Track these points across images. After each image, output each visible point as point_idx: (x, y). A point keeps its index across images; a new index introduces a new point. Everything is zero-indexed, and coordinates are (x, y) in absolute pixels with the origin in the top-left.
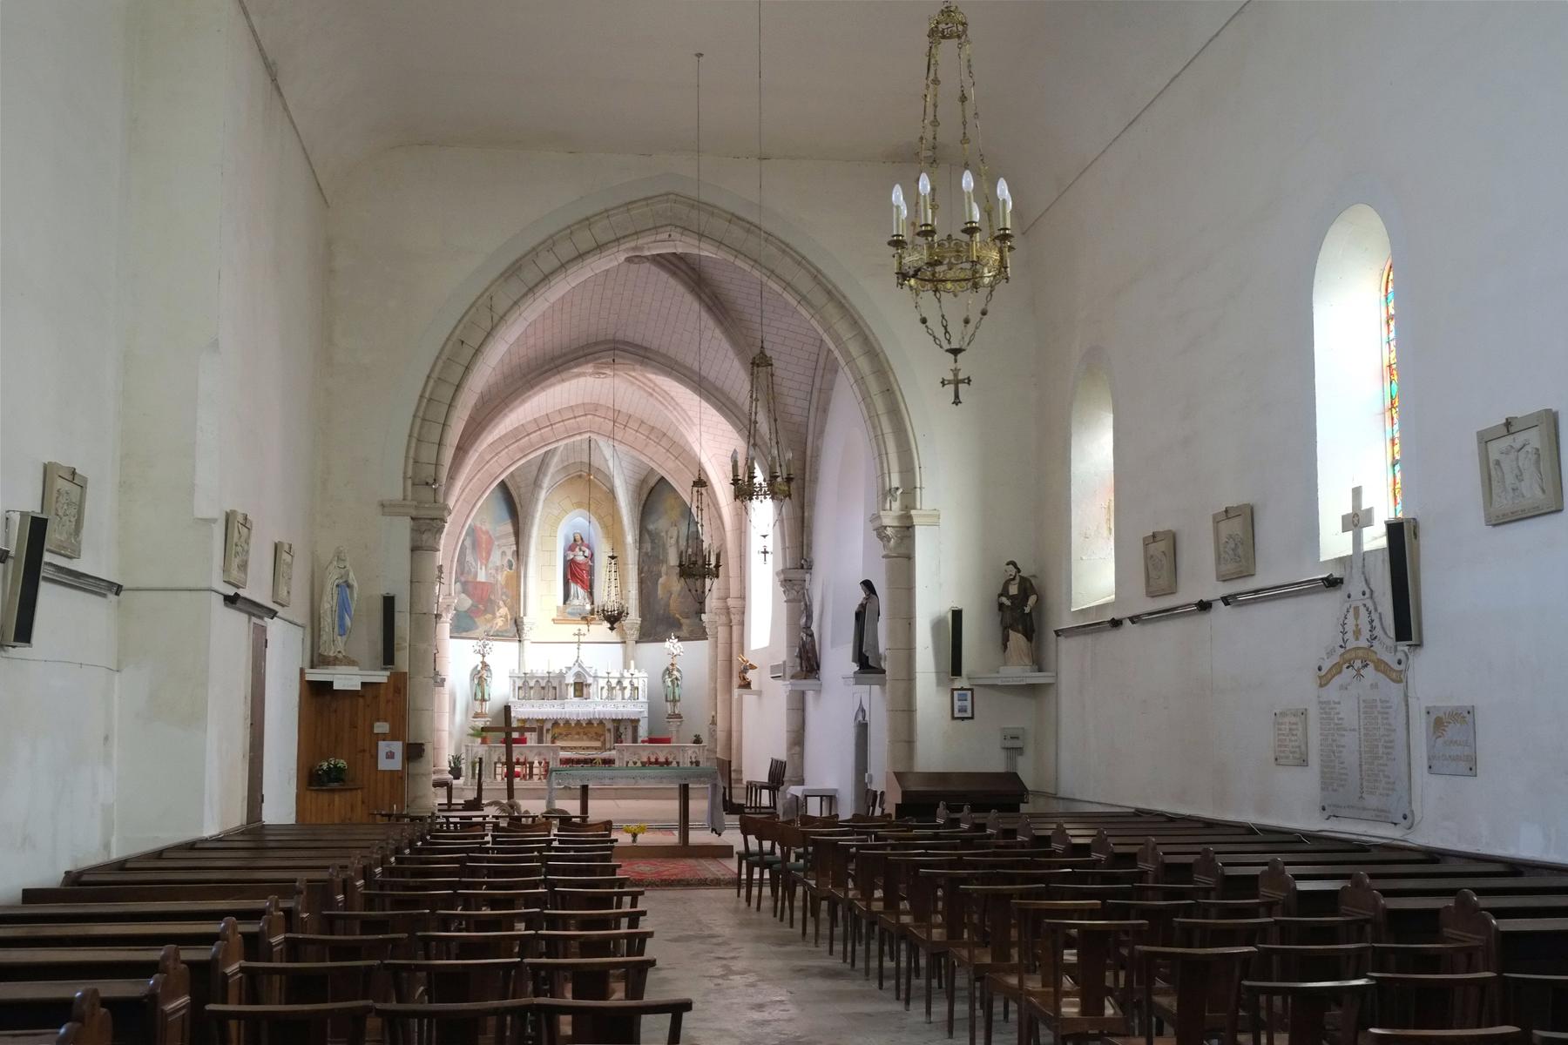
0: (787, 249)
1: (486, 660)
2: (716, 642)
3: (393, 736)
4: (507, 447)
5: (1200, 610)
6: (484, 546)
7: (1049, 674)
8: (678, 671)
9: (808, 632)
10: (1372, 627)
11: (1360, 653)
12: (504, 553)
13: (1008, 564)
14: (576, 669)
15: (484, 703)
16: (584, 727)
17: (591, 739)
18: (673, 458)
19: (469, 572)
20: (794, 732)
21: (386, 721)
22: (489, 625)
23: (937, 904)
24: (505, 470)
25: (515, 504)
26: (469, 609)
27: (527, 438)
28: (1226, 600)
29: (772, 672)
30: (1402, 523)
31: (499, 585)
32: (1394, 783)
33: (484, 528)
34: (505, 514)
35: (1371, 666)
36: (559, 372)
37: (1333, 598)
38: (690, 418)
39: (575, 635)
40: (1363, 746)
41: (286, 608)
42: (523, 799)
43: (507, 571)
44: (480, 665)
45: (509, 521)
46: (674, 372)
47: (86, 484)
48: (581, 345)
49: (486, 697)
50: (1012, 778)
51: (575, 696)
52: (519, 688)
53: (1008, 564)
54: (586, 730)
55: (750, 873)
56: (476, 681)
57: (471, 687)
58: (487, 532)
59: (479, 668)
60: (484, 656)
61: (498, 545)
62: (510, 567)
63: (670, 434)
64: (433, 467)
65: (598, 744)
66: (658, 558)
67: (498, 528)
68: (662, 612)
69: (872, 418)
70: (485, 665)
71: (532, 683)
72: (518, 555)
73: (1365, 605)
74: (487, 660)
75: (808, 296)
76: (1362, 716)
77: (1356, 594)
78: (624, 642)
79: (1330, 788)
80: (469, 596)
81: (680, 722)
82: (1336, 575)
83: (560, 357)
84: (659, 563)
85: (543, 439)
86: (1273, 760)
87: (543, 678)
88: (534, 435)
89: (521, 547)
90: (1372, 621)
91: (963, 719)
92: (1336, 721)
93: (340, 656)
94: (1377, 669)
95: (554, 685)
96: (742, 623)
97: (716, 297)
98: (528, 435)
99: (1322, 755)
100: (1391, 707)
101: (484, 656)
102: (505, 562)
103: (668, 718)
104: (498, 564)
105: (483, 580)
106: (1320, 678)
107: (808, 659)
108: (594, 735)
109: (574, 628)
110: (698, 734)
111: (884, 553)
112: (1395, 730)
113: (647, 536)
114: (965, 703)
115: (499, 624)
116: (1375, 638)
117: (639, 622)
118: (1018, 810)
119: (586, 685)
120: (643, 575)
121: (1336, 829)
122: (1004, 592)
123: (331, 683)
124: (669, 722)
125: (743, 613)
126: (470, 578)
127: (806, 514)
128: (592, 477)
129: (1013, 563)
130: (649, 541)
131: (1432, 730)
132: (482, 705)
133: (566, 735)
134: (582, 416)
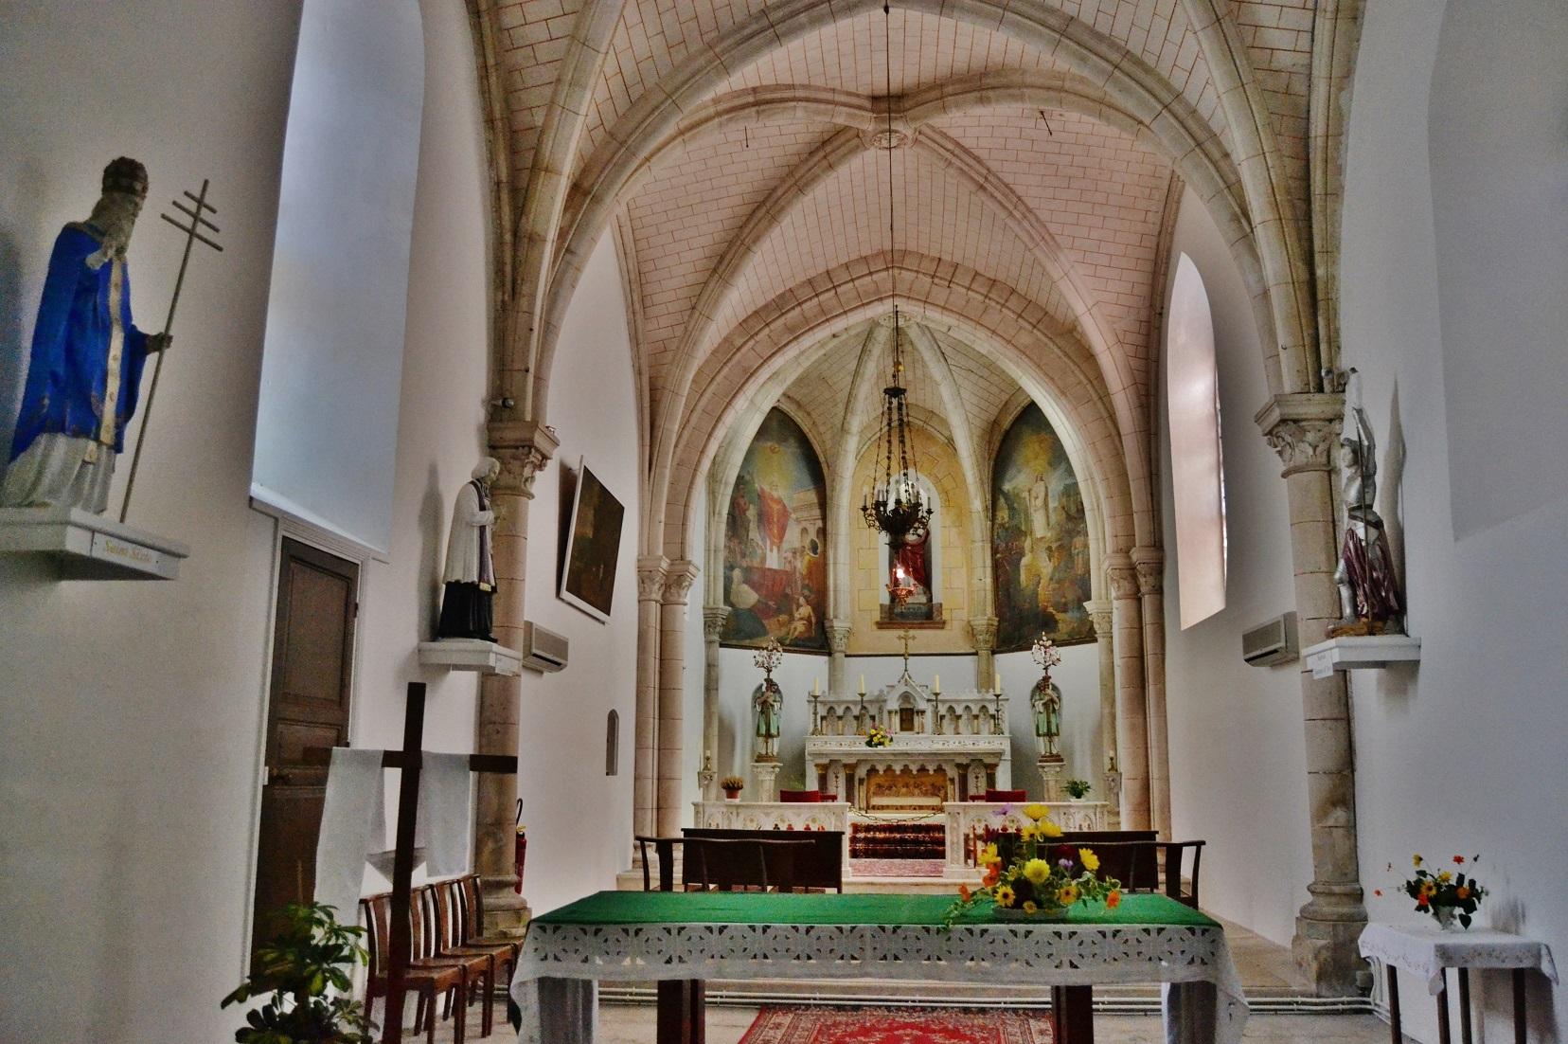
1: (772, 676)
2: (1111, 643)
6: (775, 520)
9: (1370, 517)
12: (804, 530)
14: (903, 689)
15: (770, 740)
16: (914, 777)
17: (925, 794)
18: (1030, 327)
22: (784, 630)
23: (532, 419)
26: (753, 606)
27: (798, 310)
31: (798, 575)
33: (775, 494)
34: (805, 478)
36: (778, 38)
43: (809, 555)
44: (765, 685)
46: (1009, 15)
49: (773, 731)
51: (902, 729)
52: (823, 718)
56: (759, 709)
57: (754, 715)
58: (779, 501)
60: (769, 671)
62: (814, 549)
71: (840, 711)
74: (774, 676)
78: (976, 654)
81: (1061, 767)
87: (855, 703)
88: (808, 303)
89: (829, 524)
95: (872, 713)
98: (800, 304)
101: (769, 671)
102: (807, 543)
103: (1040, 761)
104: (797, 544)
108: (929, 787)
110: (1462, 864)
113: (1002, 500)
117: (996, 623)
119: (918, 712)
120: (999, 555)
124: (1043, 767)
126: (756, 563)
127: (1320, 272)
132: (767, 743)
133: (890, 788)
134: (883, 270)
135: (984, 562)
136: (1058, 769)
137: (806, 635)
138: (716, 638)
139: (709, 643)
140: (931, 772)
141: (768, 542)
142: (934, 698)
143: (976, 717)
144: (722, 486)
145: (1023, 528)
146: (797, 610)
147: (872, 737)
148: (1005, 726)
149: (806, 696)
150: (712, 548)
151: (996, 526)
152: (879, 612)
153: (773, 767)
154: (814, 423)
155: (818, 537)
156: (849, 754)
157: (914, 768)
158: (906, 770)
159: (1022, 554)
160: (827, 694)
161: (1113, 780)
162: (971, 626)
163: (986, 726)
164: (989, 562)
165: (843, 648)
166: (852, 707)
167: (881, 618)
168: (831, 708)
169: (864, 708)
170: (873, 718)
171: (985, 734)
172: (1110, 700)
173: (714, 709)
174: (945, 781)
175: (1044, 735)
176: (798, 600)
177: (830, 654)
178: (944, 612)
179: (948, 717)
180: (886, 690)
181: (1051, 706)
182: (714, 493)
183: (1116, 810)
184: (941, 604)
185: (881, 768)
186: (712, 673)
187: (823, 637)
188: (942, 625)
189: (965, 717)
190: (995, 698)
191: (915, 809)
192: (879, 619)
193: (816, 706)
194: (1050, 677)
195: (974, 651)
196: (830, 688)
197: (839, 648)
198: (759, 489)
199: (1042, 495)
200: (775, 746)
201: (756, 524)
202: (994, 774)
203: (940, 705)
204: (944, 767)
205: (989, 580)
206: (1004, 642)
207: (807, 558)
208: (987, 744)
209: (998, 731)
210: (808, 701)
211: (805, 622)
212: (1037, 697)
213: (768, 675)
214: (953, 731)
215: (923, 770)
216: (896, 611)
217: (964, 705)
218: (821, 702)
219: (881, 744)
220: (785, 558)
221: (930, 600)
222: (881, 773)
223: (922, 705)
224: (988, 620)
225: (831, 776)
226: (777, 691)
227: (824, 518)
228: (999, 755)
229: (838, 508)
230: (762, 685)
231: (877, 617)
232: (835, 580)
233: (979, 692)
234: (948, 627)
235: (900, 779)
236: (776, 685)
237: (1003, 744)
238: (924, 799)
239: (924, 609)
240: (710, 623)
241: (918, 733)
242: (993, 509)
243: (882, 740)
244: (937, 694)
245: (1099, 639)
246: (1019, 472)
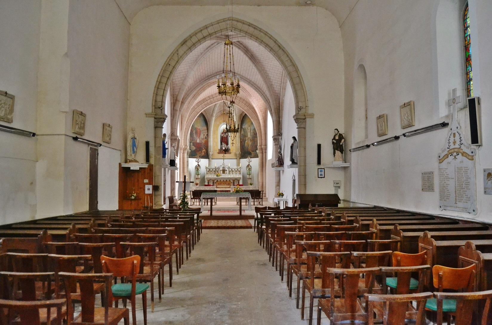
0: (266, 33)
1: (199, 164)
3: (149, 184)
4: (201, 104)
5: (396, 139)
7: (348, 163)
8: (251, 166)
10: (461, 140)
11: (456, 150)
12: (204, 135)
13: (335, 130)
14: (223, 166)
17: (227, 185)
19: (195, 140)
20: (277, 182)
21: (147, 179)
24: (201, 111)
25: (207, 121)
28: (404, 135)
29: (272, 165)
30: (474, 99)
32: (469, 198)
33: (199, 128)
34: (204, 124)
35: (460, 154)
37: (445, 130)
38: (250, 94)
39: (223, 157)
40: (456, 184)
41: (110, 144)
43: (205, 140)
45: (206, 126)
47: (86, 116)
48: (216, 72)
49: (199, 174)
50: (336, 196)
53: (335, 130)
55: (258, 224)
56: (196, 170)
57: (195, 171)
58: (199, 129)
59: (197, 166)
60: (198, 163)
61: (203, 133)
63: (245, 100)
64: (161, 103)
67: (202, 128)
70: (198, 165)
71: (211, 170)
72: (208, 135)
73: (458, 132)
75: (273, 48)
76: (456, 173)
77: (454, 128)
78: (237, 159)
79: (443, 200)
80: (194, 146)
82: (446, 122)
83: (210, 76)
85: (211, 102)
86: (421, 189)
87: (214, 168)
90: (461, 138)
91: (321, 178)
92: (446, 175)
93: (133, 159)
94: (462, 155)
96: (266, 152)
97: (252, 56)
98: (207, 101)
99: (440, 188)
100: (468, 169)
101: (198, 163)
102: (205, 137)
105: (199, 142)
106: (440, 160)
107: (280, 161)
109: (222, 155)
111: (297, 127)
112: (470, 178)
113: (242, 130)
114: (322, 173)
116: (462, 144)
118: (337, 206)
121: (445, 214)
122: (334, 139)
123: (130, 168)
125: (266, 150)
127: (280, 120)
128: (224, 112)
129: (337, 130)
131: (486, 177)
133: (220, 184)
148: (242, 173)
156: (213, 178)
157: (225, 180)
159: (246, 140)
163: (238, 173)
166: (214, 169)
170: (217, 171)
177: (209, 159)
204: (230, 180)
209: (240, 174)
215: (227, 181)
223: (227, 169)
227: (208, 132)
231: (218, 151)
234: (232, 153)
237: (241, 176)
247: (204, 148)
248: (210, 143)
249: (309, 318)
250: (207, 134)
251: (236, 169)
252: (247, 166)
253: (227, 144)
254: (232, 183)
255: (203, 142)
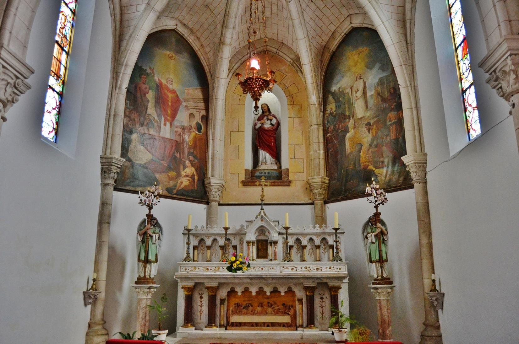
1: (152, 212)
6: (170, 104)
12: (192, 115)
14: (259, 223)
15: (148, 265)
16: (268, 298)
17: (277, 313)
31: (185, 145)
33: (171, 87)
42: (450, 155)
43: (195, 133)
49: (151, 257)
51: (258, 257)
52: (195, 248)
54: (272, 300)
58: (174, 92)
60: (150, 208)
61: (186, 106)
62: (199, 128)
65: (286, 319)
66: (344, 115)
68: (351, 166)
69: (485, 64)
70: (151, 218)
71: (209, 242)
78: (312, 204)
84: (345, 119)
87: (220, 235)
102: (194, 124)
103: (373, 284)
104: (186, 124)
108: (281, 306)
113: (331, 98)
115: (184, 184)
117: (327, 182)
119: (271, 243)
124: (376, 289)
130: (333, 101)
132: (145, 267)
133: (246, 307)
135: (319, 140)
136: (389, 290)
137: (190, 188)
138: (112, 182)
139: (104, 186)
140: (283, 294)
141: (163, 119)
142: (284, 231)
143: (318, 247)
144: (123, 67)
145: (347, 113)
146: (184, 169)
147: (232, 263)
148: (342, 255)
149: (182, 230)
150: (113, 113)
151: (327, 115)
152: (244, 174)
153: (149, 288)
154: (202, 45)
155: (202, 121)
156: (210, 278)
157: (268, 290)
158: (261, 291)
159: (346, 131)
160: (205, 228)
161: (436, 300)
162: (310, 184)
163: (326, 254)
164: (321, 140)
165: (217, 199)
166: (218, 238)
167: (246, 178)
168: (202, 240)
169: (228, 240)
170: (235, 247)
171: (325, 261)
172: (428, 233)
173: (105, 238)
174: (294, 301)
175: (377, 262)
176: (185, 162)
177: (208, 203)
178: (290, 174)
179: (295, 247)
180: (245, 224)
181: (381, 237)
182: (117, 72)
183: (437, 324)
184: (288, 170)
185: (239, 290)
186: (105, 210)
187: (203, 190)
188: (288, 183)
189: (309, 247)
190: (334, 231)
191: (268, 326)
192: (244, 179)
193: (188, 238)
194: (380, 214)
195: (310, 202)
196: (207, 225)
197: (215, 199)
198: (158, 80)
199: (361, 88)
200: (153, 270)
201: (153, 105)
202: (337, 296)
203: (289, 237)
204: (294, 289)
205: (322, 152)
206: (333, 194)
207: (193, 135)
208: (328, 269)
209: (336, 258)
210: (183, 234)
211: (190, 179)
212: (369, 230)
213: (150, 212)
214: (299, 259)
215: (275, 291)
216: (256, 174)
217: (309, 237)
218: (194, 235)
219: (240, 269)
220: (176, 132)
221: (280, 167)
222: (240, 294)
223: (275, 236)
224: (322, 178)
225: (196, 297)
226: (157, 225)
227: (207, 109)
228: (340, 278)
229: (217, 101)
230: (146, 220)
231: (243, 177)
232: (213, 150)
233: (320, 227)
234: (292, 185)
235: (256, 300)
236: (156, 219)
237: (344, 271)
238: (274, 317)
239: (276, 174)
240: (105, 170)
241: (271, 260)
242: (324, 104)
243: (240, 266)
244: (287, 228)
245: (415, 185)
246: (343, 77)
247: (191, 161)
248: (213, 147)
249: (116, 22)
250: (203, 117)
251: (314, 238)
252: (366, 219)
253: (277, 155)
254: (300, 301)
255: (186, 137)
